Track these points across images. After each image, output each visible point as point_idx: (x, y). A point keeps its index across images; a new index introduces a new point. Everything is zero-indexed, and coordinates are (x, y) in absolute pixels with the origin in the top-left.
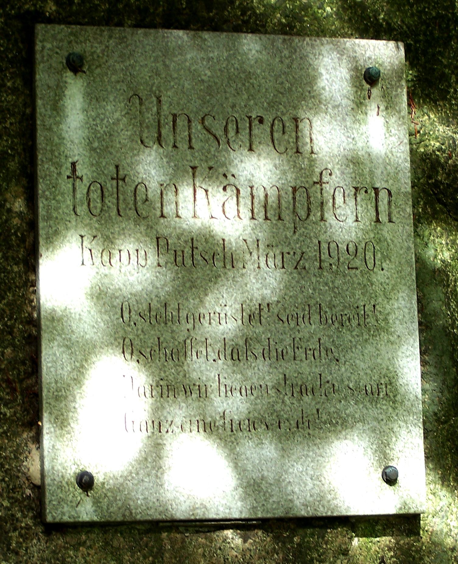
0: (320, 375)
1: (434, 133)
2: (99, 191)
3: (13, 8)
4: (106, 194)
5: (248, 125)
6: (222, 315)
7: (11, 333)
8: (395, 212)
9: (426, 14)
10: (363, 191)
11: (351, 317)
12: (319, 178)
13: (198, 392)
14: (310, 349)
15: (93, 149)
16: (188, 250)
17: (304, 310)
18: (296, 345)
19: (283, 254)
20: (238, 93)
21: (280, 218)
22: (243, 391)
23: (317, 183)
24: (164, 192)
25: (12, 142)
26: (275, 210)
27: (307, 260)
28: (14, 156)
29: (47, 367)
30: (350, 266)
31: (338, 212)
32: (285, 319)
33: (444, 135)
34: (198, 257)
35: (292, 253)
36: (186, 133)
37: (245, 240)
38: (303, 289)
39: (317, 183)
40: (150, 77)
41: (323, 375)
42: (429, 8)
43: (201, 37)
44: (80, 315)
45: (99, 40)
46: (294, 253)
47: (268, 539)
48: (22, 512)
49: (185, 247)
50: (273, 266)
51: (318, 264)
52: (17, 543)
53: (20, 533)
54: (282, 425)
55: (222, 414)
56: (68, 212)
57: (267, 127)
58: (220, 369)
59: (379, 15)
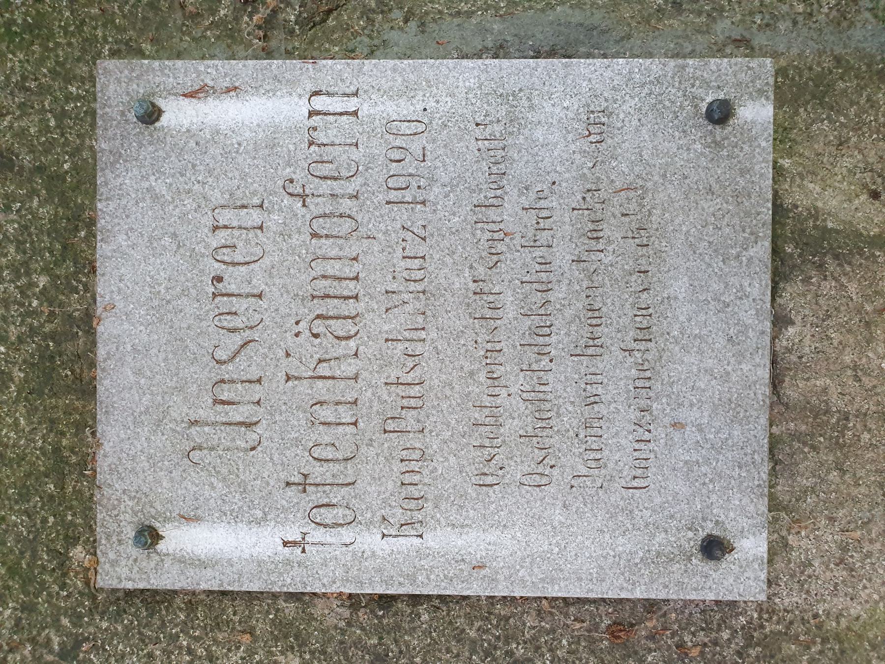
0: (574, 209)
1: (230, 23)
2: (322, 510)
3: (82, 604)
4: (326, 501)
5: (225, 298)
6: (489, 346)
7: (507, 619)
8: (342, 88)
9: (67, 25)
10: (315, 134)
11: (493, 160)
12: (297, 199)
13: (595, 386)
14: (538, 223)
15: (265, 518)
16: (401, 390)
17: (482, 229)
18: (532, 244)
19: (404, 257)
20: (181, 311)
21: (355, 259)
22: (594, 322)
23: (304, 201)
24: (322, 420)
25: (259, 612)
26: (344, 265)
27: (413, 223)
28: (278, 610)
29: (559, 591)
30: (421, 159)
31: (345, 173)
32: (495, 258)
33: (232, 8)
34: (409, 379)
35: (404, 244)
36: (239, 386)
37: (387, 310)
38: (454, 230)
39: (304, 201)
40: (163, 434)
41: (574, 206)
42: (60, 21)
43: (105, 360)
44: (490, 544)
45: (116, 502)
46: (403, 240)
47: (789, 289)
48: (738, 614)
49: (398, 395)
50: (422, 271)
51: (419, 206)
52: (778, 623)
53: (767, 621)
54: (643, 269)
55: (627, 353)
56: (350, 554)
57: (228, 272)
58: (563, 354)
59: (71, 93)
